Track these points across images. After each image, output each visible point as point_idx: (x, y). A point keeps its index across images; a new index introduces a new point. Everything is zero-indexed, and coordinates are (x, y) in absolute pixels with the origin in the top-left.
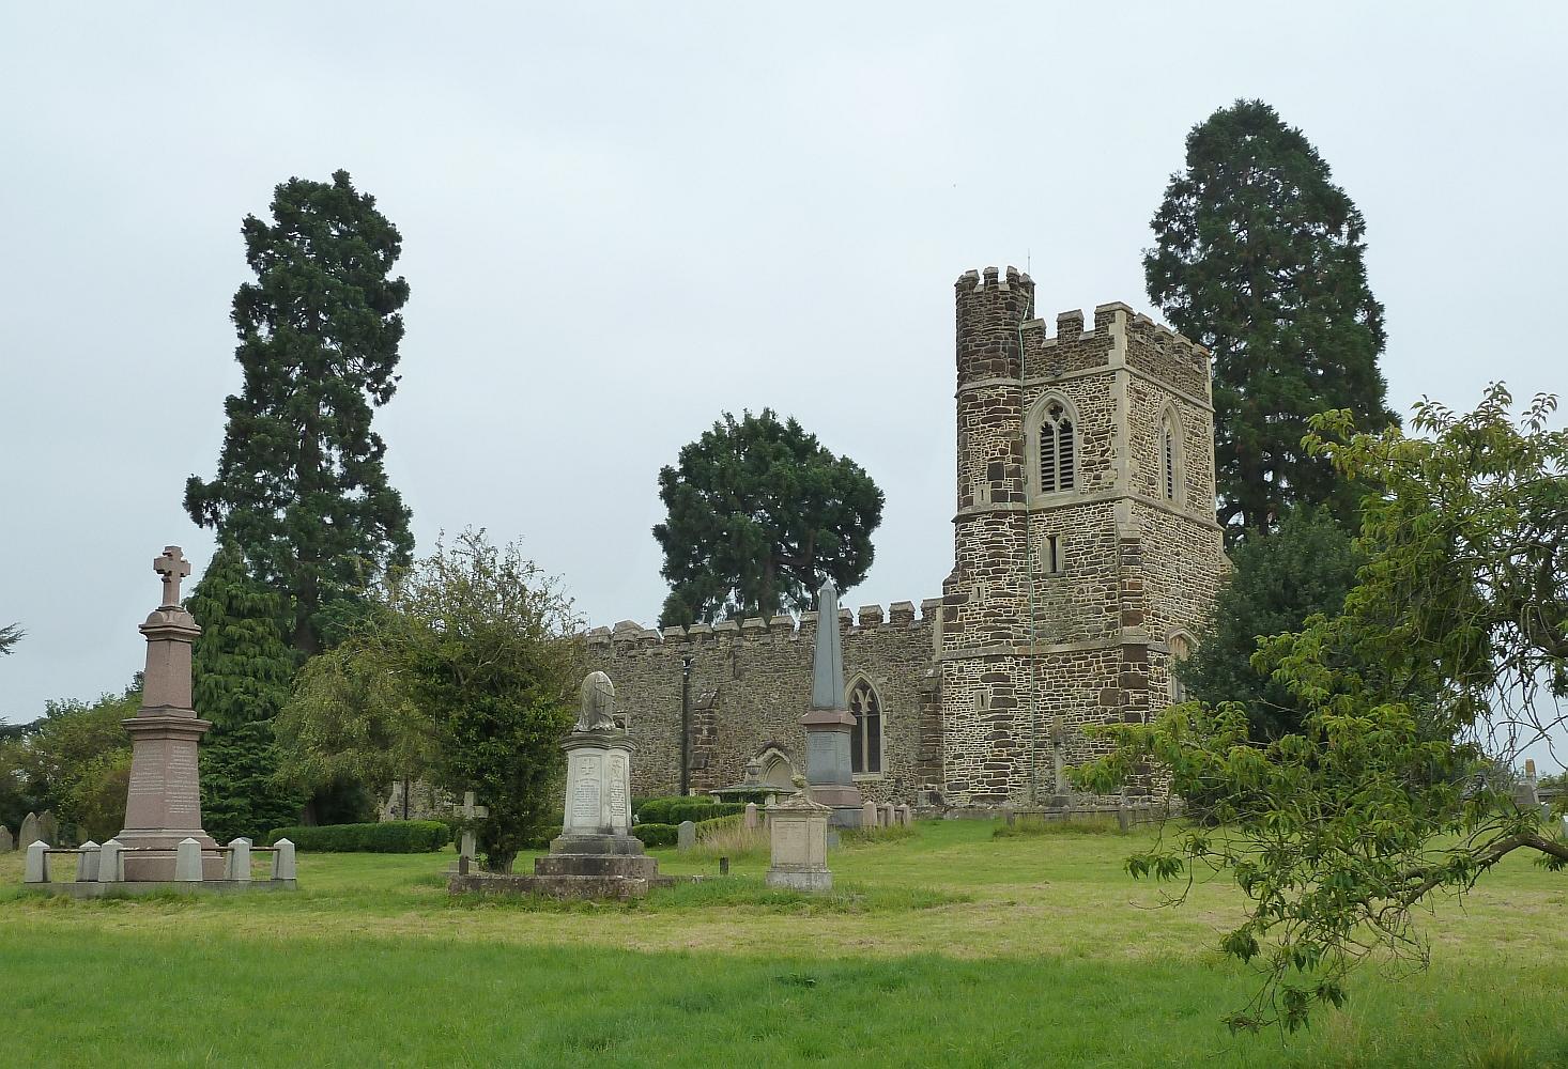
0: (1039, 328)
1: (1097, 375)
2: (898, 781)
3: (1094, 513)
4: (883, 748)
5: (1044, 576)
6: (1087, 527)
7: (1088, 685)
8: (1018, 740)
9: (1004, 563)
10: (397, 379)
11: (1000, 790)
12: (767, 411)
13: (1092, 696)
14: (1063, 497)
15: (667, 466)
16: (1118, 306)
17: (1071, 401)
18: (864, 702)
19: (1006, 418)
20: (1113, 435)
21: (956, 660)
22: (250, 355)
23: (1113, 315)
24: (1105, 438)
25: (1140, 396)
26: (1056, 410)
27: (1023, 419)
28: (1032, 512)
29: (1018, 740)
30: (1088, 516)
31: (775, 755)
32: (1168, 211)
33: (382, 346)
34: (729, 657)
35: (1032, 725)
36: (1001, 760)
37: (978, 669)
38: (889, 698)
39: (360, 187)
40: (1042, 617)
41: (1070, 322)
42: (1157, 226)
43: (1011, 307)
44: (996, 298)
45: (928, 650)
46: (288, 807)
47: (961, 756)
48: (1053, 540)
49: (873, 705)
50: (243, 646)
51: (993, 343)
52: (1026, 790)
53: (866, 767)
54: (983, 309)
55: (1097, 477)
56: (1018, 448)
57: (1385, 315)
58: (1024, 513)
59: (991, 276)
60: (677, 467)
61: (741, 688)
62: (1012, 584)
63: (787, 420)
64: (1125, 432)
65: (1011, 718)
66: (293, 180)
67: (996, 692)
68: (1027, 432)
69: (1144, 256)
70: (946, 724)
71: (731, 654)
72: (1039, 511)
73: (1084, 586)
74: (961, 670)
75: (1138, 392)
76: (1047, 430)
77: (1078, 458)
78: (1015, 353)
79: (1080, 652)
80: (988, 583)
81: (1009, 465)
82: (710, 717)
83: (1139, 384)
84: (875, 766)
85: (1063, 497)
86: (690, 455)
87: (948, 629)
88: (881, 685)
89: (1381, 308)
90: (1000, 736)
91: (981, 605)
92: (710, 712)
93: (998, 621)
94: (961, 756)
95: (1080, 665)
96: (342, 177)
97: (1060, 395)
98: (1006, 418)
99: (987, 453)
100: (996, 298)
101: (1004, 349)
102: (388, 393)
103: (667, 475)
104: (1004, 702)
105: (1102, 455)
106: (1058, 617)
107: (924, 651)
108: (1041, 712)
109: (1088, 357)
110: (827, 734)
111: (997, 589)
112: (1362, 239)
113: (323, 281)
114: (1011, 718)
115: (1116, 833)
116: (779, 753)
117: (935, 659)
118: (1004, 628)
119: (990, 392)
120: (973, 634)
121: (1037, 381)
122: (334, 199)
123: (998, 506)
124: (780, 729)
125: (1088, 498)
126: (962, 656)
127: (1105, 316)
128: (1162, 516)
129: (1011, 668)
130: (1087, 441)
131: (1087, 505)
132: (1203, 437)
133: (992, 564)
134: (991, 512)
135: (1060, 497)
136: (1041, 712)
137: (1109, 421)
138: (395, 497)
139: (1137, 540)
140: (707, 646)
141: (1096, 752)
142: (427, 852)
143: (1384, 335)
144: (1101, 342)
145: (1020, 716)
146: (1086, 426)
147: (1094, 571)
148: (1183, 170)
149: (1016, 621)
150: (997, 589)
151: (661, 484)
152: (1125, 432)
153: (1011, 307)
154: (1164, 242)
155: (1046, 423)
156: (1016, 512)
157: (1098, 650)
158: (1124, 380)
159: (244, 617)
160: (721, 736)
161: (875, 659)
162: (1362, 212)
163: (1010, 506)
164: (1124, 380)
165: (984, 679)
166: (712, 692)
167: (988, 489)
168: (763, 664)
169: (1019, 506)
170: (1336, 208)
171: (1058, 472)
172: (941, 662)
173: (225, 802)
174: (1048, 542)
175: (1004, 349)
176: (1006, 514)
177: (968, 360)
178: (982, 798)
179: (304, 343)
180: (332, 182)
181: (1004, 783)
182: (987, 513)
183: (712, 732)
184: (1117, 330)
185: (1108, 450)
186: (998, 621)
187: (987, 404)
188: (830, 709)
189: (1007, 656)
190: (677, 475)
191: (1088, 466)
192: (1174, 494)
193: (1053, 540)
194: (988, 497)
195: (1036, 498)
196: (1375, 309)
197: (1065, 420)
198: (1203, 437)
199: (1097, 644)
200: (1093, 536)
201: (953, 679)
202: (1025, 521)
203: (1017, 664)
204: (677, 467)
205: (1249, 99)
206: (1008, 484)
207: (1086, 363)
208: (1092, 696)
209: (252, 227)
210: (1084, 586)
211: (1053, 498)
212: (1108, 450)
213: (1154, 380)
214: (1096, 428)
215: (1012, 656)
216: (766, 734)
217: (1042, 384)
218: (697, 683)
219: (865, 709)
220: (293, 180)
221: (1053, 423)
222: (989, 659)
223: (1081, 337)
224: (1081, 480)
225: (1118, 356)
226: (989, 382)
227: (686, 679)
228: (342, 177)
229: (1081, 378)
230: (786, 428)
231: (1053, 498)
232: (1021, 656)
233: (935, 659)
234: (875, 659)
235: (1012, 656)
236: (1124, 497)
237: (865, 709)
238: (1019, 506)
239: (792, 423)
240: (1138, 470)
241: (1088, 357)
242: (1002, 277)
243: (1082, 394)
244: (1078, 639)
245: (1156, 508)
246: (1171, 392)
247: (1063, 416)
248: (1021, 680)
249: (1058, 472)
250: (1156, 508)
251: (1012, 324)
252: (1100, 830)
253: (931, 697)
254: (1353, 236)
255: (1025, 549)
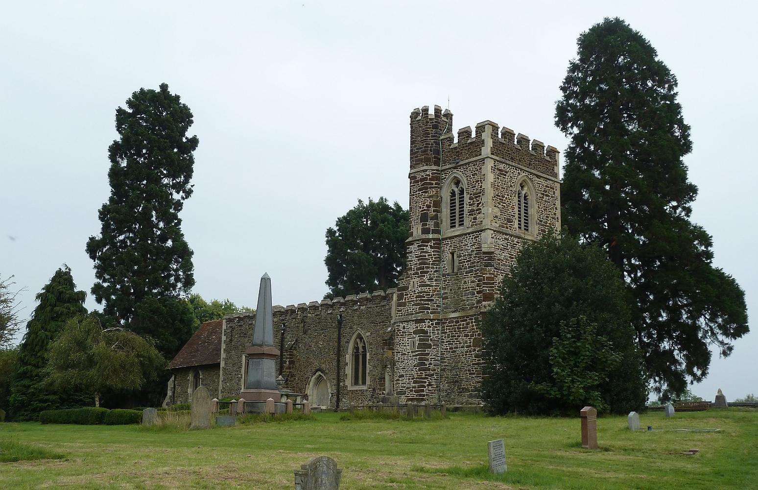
0: (449, 138)
1: (476, 161)
2: (374, 390)
3: (472, 239)
4: (368, 371)
5: (448, 275)
6: (469, 245)
7: (466, 336)
8: (432, 367)
9: (426, 267)
10: (192, 186)
11: (420, 395)
12: (382, 198)
13: (468, 342)
14: (460, 230)
15: (330, 228)
16: (486, 123)
17: (464, 178)
18: (360, 345)
19: (430, 188)
20: (483, 194)
21: (402, 322)
22: (115, 175)
23: (484, 128)
24: (479, 196)
25: (502, 173)
26: (457, 182)
27: (441, 188)
28: (443, 239)
29: (432, 367)
30: (469, 240)
31: (320, 375)
32: (569, 80)
33: (186, 168)
34: (302, 323)
35: (439, 358)
36: (422, 378)
37: (412, 327)
38: (371, 344)
39: (172, 91)
40: (446, 298)
41: (465, 133)
42: (562, 89)
43: (435, 127)
44: (427, 122)
45: (389, 317)
46: (81, 400)
47: (402, 376)
48: (452, 254)
49: (364, 348)
50: (63, 317)
51: (425, 147)
52: (436, 395)
53: (360, 382)
54: (420, 129)
55: (475, 219)
56: (437, 204)
57: (690, 132)
58: (438, 239)
59: (426, 110)
60: (336, 228)
61: (307, 339)
62: (430, 279)
63: (394, 203)
64: (490, 192)
65: (428, 354)
66: (142, 89)
67: (420, 340)
68: (442, 195)
69: (556, 105)
70: (396, 358)
71: (303, 321)
72: (446, 239)
73: (466, 280)
74: (404, 328)
75: (500, 170)
76: (453, 194)
77: (466, 208)
78: (437, 152)
79: (463, 317)
80: (418, 279)
81: (432, 213)
82: (290, 355)
83: (502, 166)
84: (364, 383)
85: (460, 230)
86: (341, 222)
87: (399, 305)
88: (368, 336)
89: (689, 128)
90: (421, 365)
91: (415, 291)
92: (290, 352)
93: (423, 300)
94: (402, 376)
95: (463, 324)
96: (164, 87)
97: (459, 174)
98: (430, 188)
99: (420, 207)
100: (427, 122)
101: (431, 150)
102: (188, 193)
103: (330, 232)
104: (424, 345)
105: (478, 206)
106: (454, 297)
107: (387, 318)
108: (444, 351)
109: (472, 152)
110: (258, 360)
111: (422, 282)
112: (676, 90)
113: (154, 141)
114: (428, 354)
115: (404, 419)
116: (321, 374)
117: (392, 322)
118: (426, 304)
119: (423, 174)
120: (411, 308)
121: (447, 167)
122: (156, 97)
123: (424, 236)
124: (322, 361)
125: (470, 230)
126: (405, 320)
127: (480, 128)
128: (516, 240)
129: (429, 327)
130: (471, 199)
131: (469, 234)
132: (552, 197)
133: (420, 268)
134: (420, 240)
135: (458, 231)
136: (444, 351)
137: (481, 187)
138: (185, 245)
139: (493, 253)
140: (293, 316)
141: (470, 374)
142: (97, 424)
143: (691, 142)
144: (480, 143)
145: (433, 353)
146: (471, 190)
147: (471, 271)
148: (576, 58)
149: (432, 300)
150: (422, 282)
151: (327, 237)
152: (490, 192)
153: (435, 127)
154: (568, 98)
155: (453, 190)
156: (434, 239)
157: (472, 316)
158: (489, 164)
159: (65, 302)
160: (297, 365)
161: (365, 322)
162: (675, 75)
163: (431, 236)
164: (489, 164)
165: (415, 333)
166: (293, 341)
167: (420, 227)
168: (316, 326)
169: (436, 236)
170: (662, 74)
171: (456, 219)
172: (395, 323)
173: (46, 397)
174: (450, 255)
175: (431, 150)
176: (428, 240)
177: (416, 158)
178: (412, 400)
179: (138, 169)
180: (158, 90)
181: (423, 391)
182: (418, 240)
183: (291, 362)
184: (486, 135)
185: (480, 203)
186: (423, 300)
187: (421, 180)
188: (261, 346)
189: (427, 319)
190: (335, 232)
191: (471, 212)
192: (530, 229)
193: (452, 254)
194: (420, 231)
195: (447, 231)
196: (685, 129)
197: (462, 188)
198: (552, 197)
199: (471, 312)
200: (472, 251)
201: (400, 333)
202: (439, 244)
203: (432, 324)
204: (336, 228)
205: (612, 17)
206: (431, 224)
207: (471, 156)
208: (468, 342)
209: (120, 112)
210: (466, 280)
211: (454, 231)
212: (480, 203)
213: (514, 164)
214: (475, 191)
215: (430, 319)
216: (316, 363)
217: (450, 168)
218: (288, 337)
219: (361, 350)
220: (142, 89)
221: (456, 189)
222: (418, 321)
223: (469, 141)
224: (467, 221)
225: (486, 150)
226: (422, 169)
227: (283, 334)
228: (164, 87)
229: (469, 163)
230: (393, 207)
231: (454, 231)
232: (435, 320)
233: (392, 322)
234: (365, 322)
235: (430, 319)
236: (487, 229)
237: (361, 350)
238: (436, 236)
239: (396, 205)
240: (499, 214)
241: (472, 152)
242: (431, 112)
243: (469, 173)
244: (463, 310)
245: (511, 236)
246: (526, 171)
247: (460, 185)
248: (434, 334)
249: (456, 219)
250: (511, 236)
251: (436, 137)
252: (395, 417)
253: (389, 343)
254: (670, 88)
255: (439, 260)
